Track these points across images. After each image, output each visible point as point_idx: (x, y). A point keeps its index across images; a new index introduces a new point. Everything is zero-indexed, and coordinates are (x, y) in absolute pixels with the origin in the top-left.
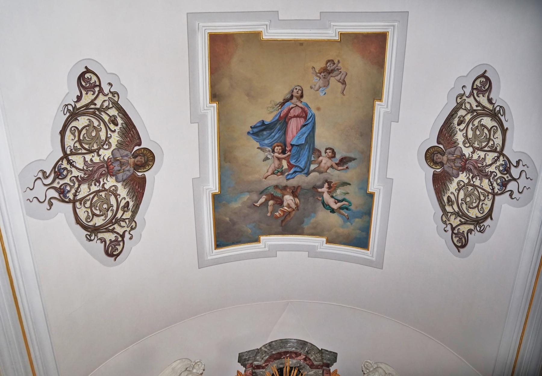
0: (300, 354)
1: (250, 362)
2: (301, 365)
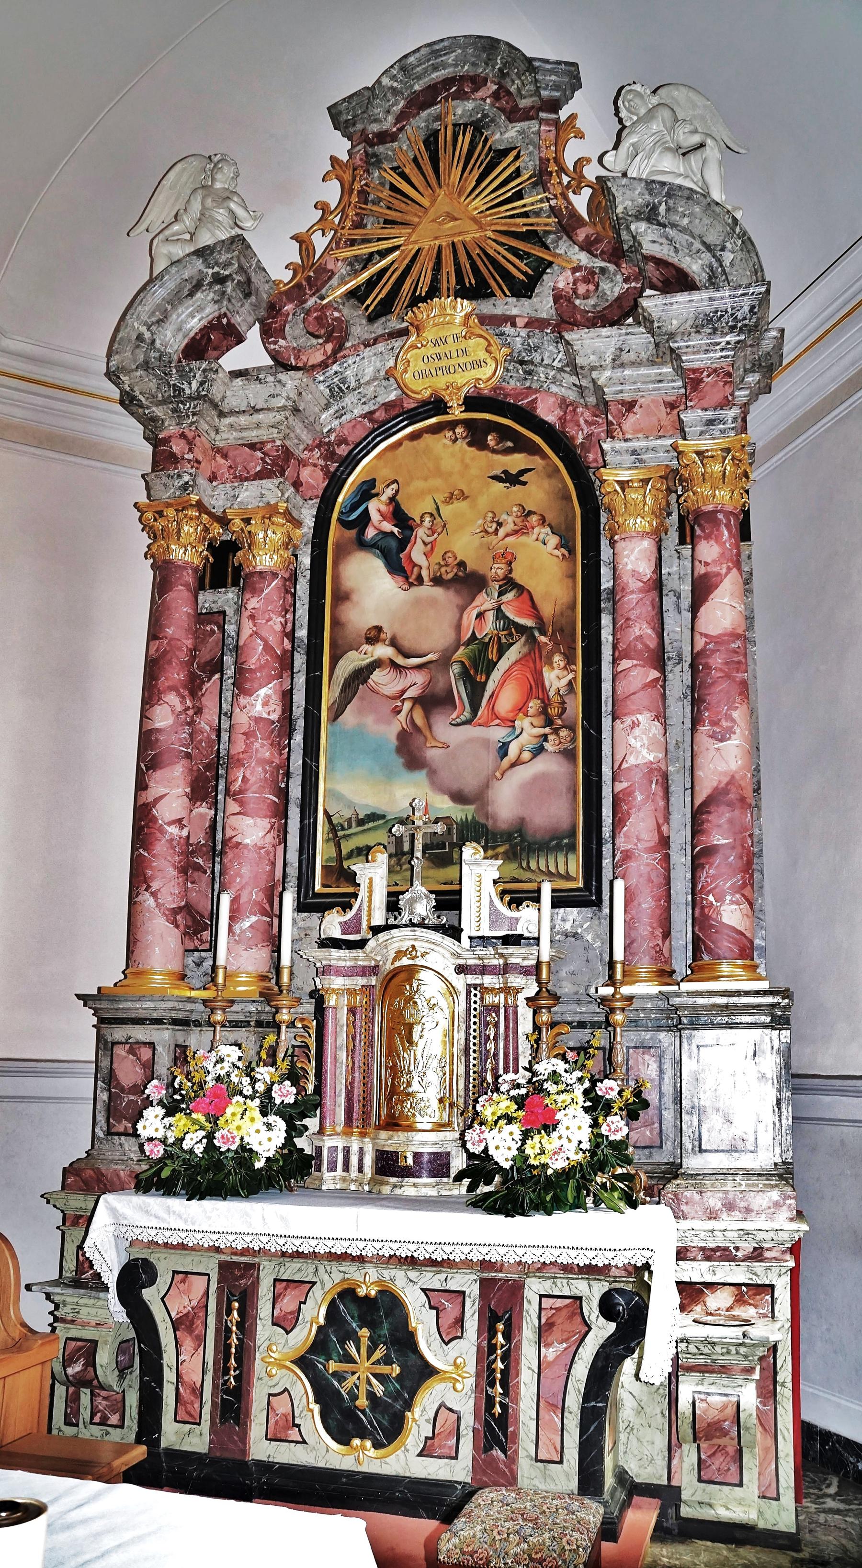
0: (485, 81)
1: (359, 127)
2: (485, 116)
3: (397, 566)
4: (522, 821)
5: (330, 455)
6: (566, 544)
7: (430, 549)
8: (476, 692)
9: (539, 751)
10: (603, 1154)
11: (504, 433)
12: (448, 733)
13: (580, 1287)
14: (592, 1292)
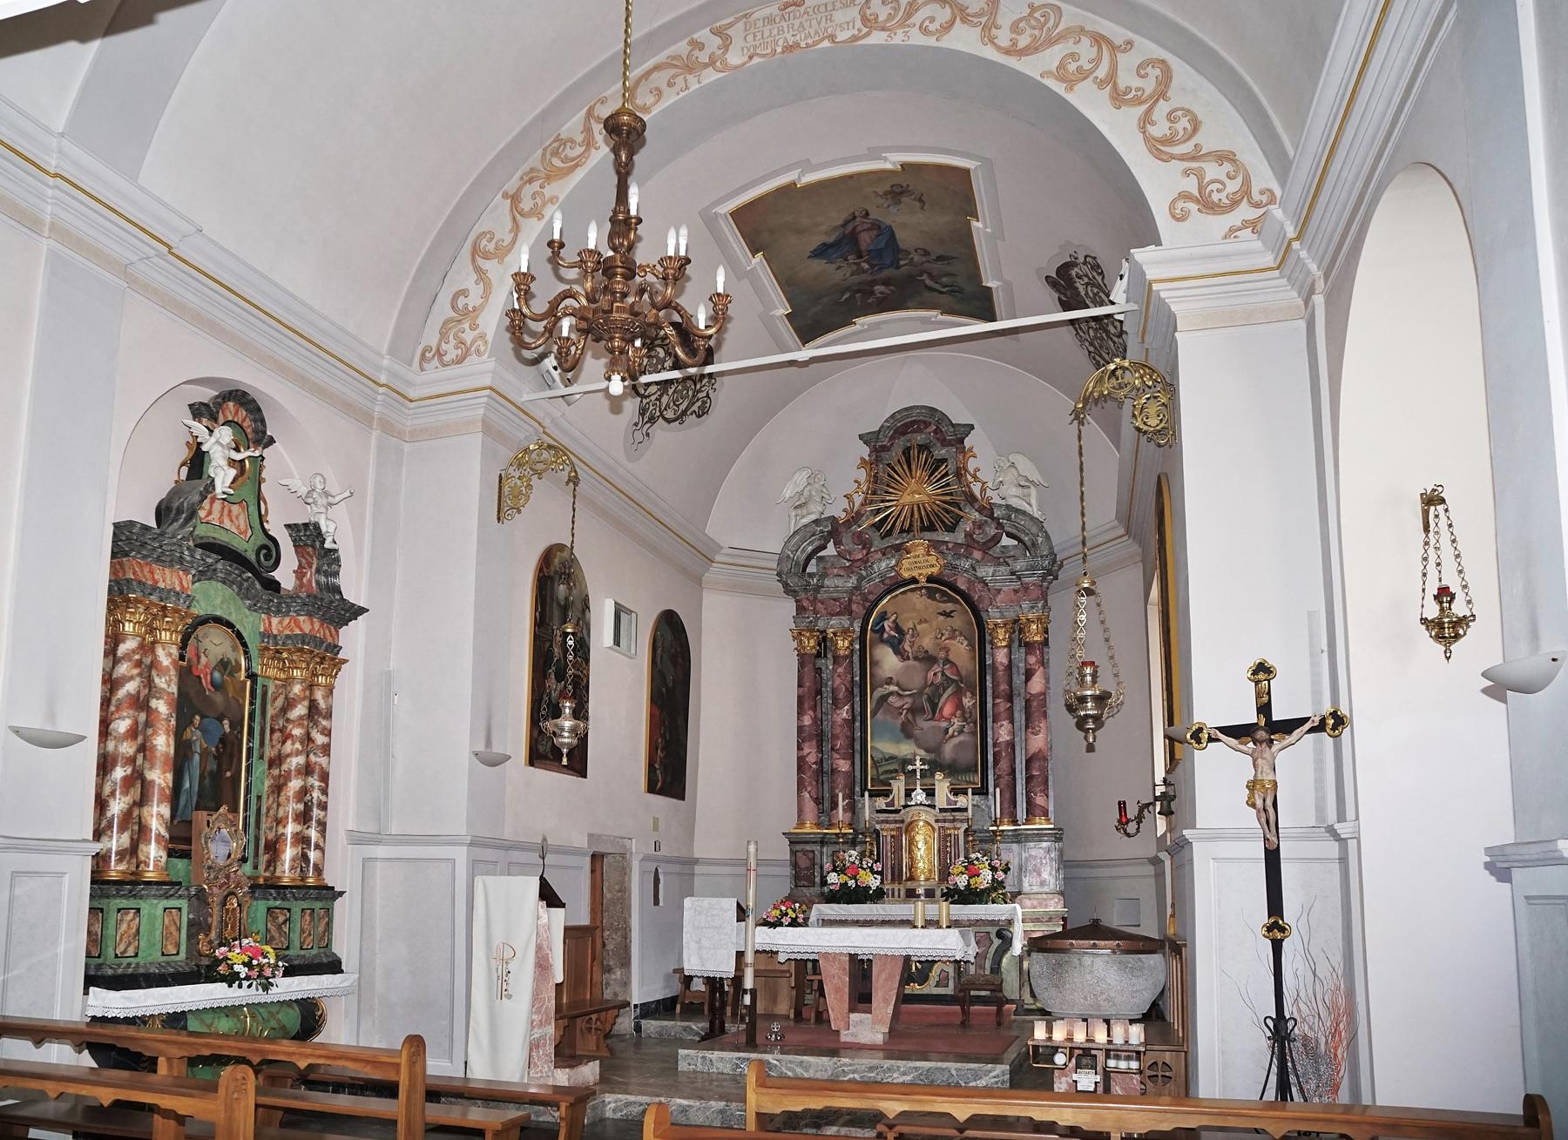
3: (898, 652)
4: (954, 760)
5: (866, 599)
6: (971, 644)
7: (912, 644)
8: (934, 706)
9: (961, 732)
10: (997, 885)
11: (944, 594)
12: (923, 724)
13: (989, 929)
14: (993, 930)
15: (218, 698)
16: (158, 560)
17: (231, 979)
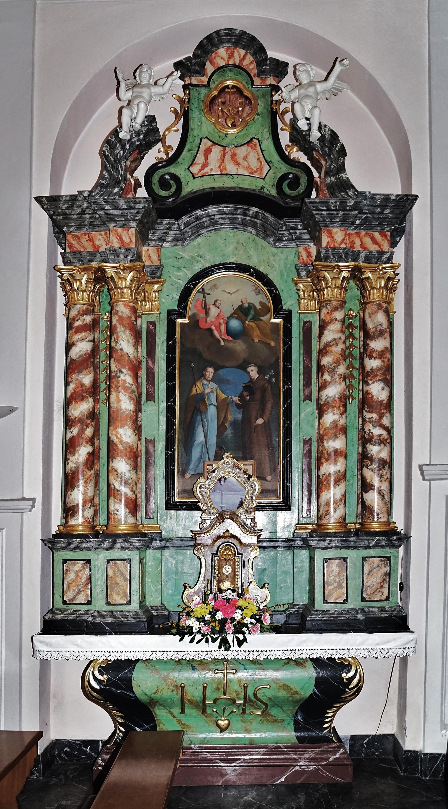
15: (239, 346)
16: (92, 225)
17: (184, 632)
